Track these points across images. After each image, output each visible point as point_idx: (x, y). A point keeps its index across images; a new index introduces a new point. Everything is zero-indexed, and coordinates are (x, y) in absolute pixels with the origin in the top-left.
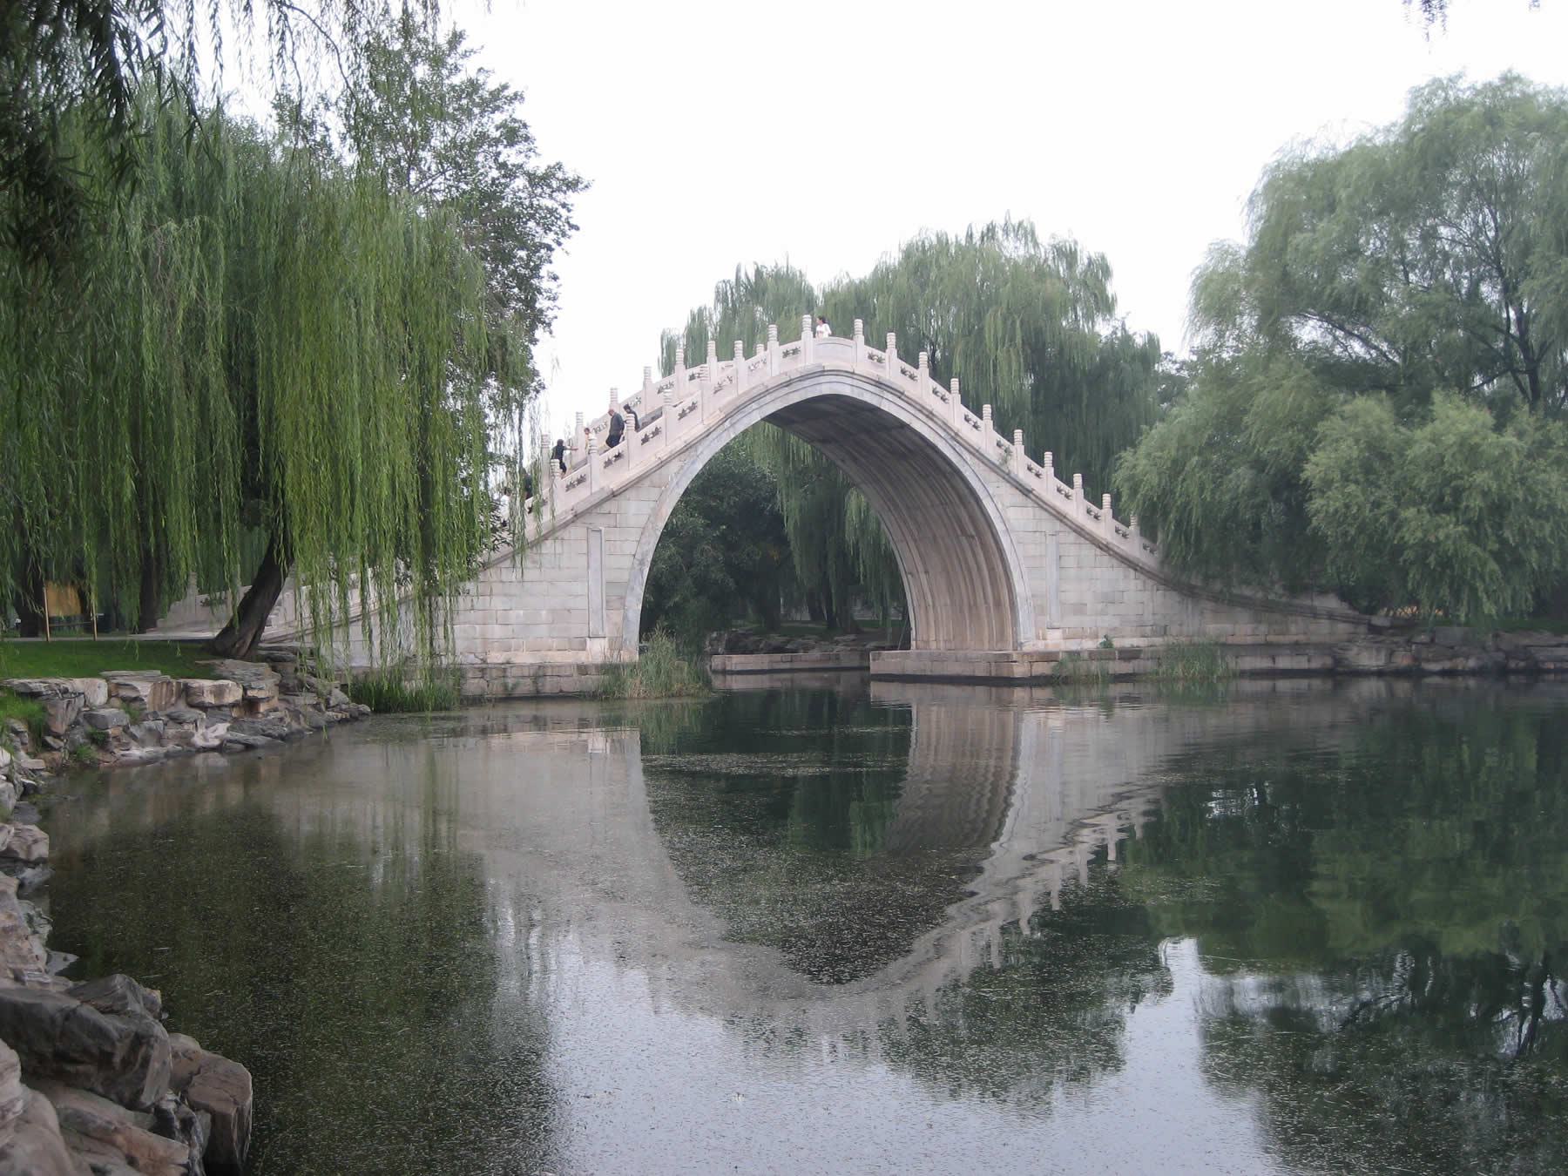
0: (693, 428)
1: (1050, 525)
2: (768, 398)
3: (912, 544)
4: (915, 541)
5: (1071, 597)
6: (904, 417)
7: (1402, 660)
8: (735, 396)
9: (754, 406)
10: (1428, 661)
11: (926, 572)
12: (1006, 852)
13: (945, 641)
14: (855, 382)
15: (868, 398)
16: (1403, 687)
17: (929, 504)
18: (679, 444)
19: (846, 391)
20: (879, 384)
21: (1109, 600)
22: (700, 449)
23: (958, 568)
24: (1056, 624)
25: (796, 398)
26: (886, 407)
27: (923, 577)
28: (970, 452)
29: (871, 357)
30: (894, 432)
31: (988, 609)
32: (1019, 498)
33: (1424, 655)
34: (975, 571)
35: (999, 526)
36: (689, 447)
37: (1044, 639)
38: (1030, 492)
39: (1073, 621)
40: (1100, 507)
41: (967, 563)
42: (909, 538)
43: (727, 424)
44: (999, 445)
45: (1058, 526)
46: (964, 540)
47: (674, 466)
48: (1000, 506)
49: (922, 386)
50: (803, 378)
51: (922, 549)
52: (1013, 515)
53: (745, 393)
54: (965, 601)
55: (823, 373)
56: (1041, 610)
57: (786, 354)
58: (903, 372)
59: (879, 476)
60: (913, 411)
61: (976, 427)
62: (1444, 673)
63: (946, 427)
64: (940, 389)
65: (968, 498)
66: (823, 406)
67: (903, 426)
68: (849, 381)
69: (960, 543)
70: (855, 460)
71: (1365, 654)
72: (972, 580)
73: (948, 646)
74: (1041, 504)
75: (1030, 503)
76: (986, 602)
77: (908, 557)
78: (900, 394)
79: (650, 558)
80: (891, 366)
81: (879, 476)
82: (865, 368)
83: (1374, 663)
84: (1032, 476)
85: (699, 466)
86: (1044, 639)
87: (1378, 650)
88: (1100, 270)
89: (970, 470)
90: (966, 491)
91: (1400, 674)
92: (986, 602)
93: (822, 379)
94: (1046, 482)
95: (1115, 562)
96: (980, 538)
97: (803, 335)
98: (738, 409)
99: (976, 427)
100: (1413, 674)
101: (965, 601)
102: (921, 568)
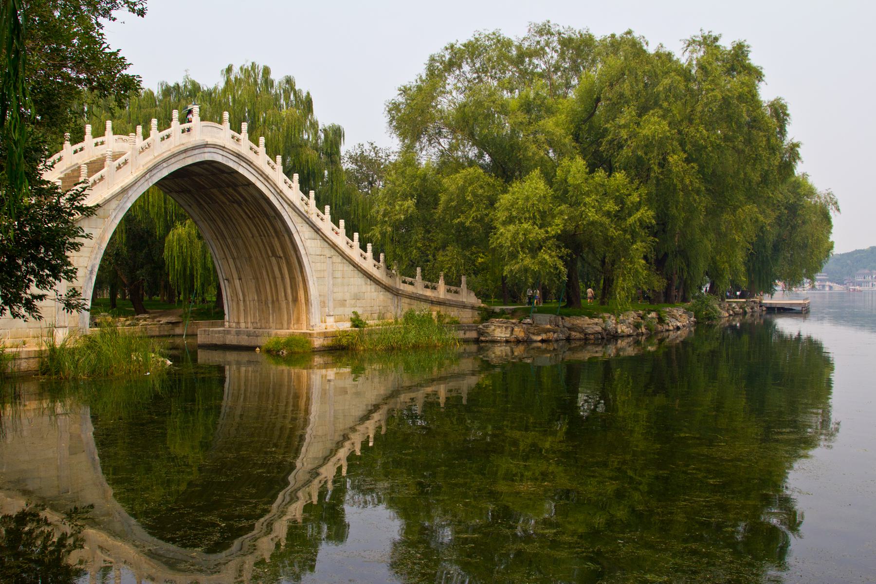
0: (126, 177)
1: (329, 252)
2: (173, 160)
3: (231, 261)
4: (234, 259)
5: (339, 296)
6: (252, 179)
7: (519, 333)
8: (152, 157)
9: (165, 165)
10: (534, 334)
11: (240, 279)
12: (304, 461)
13: (252, 323)
14: (225, 154)
15: (231, 164)
16: (519, 350)
17: (250, 235)
18: (117, 188)
19: (219, 159)
20: (239, 156)
21: (357, 297)
22: (130, 193)
23: (265, 277)
24: (331, 313)
25: (190, 161)
26: (241, 170)
27: (237, 282)
28: (289, 205)
29: (233, 137)
30: (240, 189)
31: (288, 303)
32: (312, 234)
33: (532, 331)
34: (279, 281)
35: (302, 252)
36: (124, 191)
37: (325, 322)
38: (319, 230)
39: (340, 311)
40: (353, 240)
41: (273, 272)
42: (229, 257)
43: (148, 176)
44: (302, 200)
45: (333, 252)
46: (273, 260)
47: (114, 204)
48: (303, 238)
49: (261, 159)
50: (194, 148)
51: (239, 265)
52: (309, 244)
53: (158, 156)
54: (270, 298)
55: (206, 145)
56: (323, 304)
57: (183, 131)
58: (251, 149)
59: (215, 217)
60: (257, 175)
61: (290, 187)
62: (542, 341)
63: (275, 186)
64: (271, 161)
65: (284, 233)
66: (197, 170)
67: (250, 184)
68: (221, 152)
69: (270, 261)
70: (199, 205)
71: (498, 330)
72: (276, 286)
73: (255, 325)
74: (325, 238)
75: (318, 236)
76: (286, 299)
77: (224, 269)
78: (250, 163)
79: (96, 269)
80: (244, 145)
81: (215, 217)
82: (231, 145)
83: (503, 335)
84: (319, 219)
85: (129, 205)
86: (325, 322)
87: (506, 328)
88: (740, 51)
89: (287, 214)
90: (283, 229)
91: (518, 342)
92: (286, 299)
93: (206, 150)
94: (326, 224)
95: (361, 275)
96: (286, 259)
97: (106, 133)
98: (155, 167)
99: (290, 187)
100: (527, 342)
101: (270, 298)
102: (235, 276)
